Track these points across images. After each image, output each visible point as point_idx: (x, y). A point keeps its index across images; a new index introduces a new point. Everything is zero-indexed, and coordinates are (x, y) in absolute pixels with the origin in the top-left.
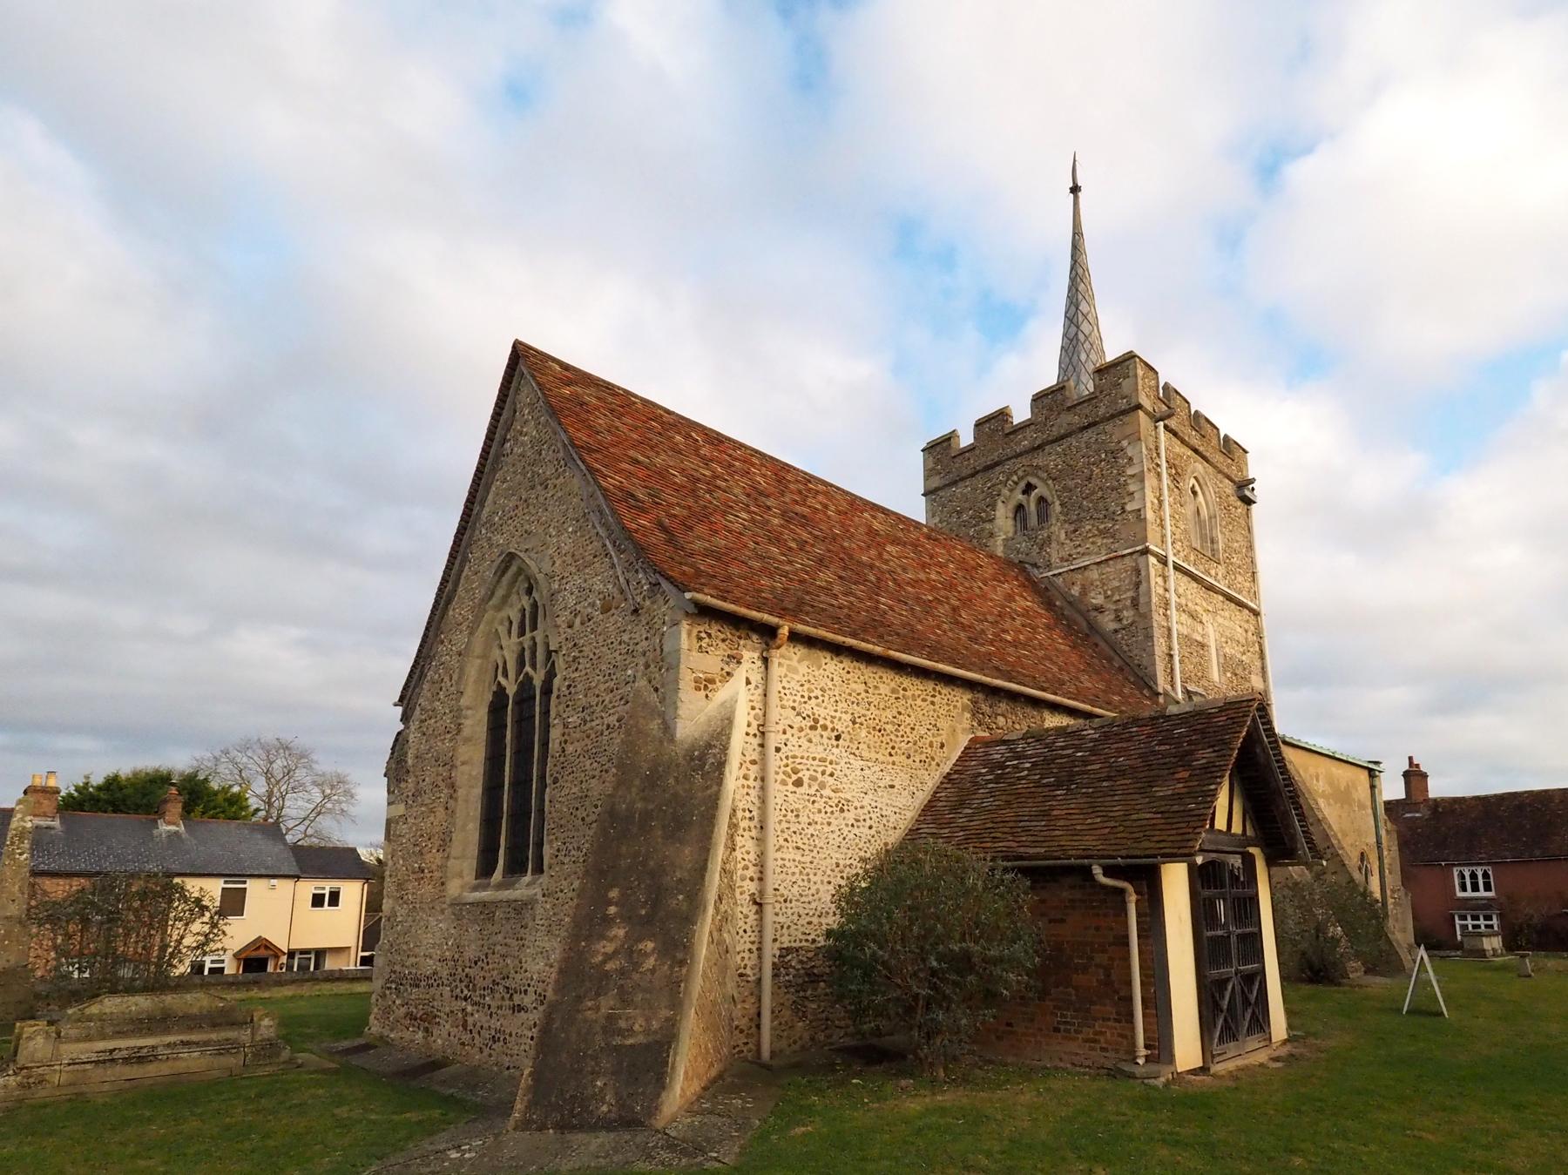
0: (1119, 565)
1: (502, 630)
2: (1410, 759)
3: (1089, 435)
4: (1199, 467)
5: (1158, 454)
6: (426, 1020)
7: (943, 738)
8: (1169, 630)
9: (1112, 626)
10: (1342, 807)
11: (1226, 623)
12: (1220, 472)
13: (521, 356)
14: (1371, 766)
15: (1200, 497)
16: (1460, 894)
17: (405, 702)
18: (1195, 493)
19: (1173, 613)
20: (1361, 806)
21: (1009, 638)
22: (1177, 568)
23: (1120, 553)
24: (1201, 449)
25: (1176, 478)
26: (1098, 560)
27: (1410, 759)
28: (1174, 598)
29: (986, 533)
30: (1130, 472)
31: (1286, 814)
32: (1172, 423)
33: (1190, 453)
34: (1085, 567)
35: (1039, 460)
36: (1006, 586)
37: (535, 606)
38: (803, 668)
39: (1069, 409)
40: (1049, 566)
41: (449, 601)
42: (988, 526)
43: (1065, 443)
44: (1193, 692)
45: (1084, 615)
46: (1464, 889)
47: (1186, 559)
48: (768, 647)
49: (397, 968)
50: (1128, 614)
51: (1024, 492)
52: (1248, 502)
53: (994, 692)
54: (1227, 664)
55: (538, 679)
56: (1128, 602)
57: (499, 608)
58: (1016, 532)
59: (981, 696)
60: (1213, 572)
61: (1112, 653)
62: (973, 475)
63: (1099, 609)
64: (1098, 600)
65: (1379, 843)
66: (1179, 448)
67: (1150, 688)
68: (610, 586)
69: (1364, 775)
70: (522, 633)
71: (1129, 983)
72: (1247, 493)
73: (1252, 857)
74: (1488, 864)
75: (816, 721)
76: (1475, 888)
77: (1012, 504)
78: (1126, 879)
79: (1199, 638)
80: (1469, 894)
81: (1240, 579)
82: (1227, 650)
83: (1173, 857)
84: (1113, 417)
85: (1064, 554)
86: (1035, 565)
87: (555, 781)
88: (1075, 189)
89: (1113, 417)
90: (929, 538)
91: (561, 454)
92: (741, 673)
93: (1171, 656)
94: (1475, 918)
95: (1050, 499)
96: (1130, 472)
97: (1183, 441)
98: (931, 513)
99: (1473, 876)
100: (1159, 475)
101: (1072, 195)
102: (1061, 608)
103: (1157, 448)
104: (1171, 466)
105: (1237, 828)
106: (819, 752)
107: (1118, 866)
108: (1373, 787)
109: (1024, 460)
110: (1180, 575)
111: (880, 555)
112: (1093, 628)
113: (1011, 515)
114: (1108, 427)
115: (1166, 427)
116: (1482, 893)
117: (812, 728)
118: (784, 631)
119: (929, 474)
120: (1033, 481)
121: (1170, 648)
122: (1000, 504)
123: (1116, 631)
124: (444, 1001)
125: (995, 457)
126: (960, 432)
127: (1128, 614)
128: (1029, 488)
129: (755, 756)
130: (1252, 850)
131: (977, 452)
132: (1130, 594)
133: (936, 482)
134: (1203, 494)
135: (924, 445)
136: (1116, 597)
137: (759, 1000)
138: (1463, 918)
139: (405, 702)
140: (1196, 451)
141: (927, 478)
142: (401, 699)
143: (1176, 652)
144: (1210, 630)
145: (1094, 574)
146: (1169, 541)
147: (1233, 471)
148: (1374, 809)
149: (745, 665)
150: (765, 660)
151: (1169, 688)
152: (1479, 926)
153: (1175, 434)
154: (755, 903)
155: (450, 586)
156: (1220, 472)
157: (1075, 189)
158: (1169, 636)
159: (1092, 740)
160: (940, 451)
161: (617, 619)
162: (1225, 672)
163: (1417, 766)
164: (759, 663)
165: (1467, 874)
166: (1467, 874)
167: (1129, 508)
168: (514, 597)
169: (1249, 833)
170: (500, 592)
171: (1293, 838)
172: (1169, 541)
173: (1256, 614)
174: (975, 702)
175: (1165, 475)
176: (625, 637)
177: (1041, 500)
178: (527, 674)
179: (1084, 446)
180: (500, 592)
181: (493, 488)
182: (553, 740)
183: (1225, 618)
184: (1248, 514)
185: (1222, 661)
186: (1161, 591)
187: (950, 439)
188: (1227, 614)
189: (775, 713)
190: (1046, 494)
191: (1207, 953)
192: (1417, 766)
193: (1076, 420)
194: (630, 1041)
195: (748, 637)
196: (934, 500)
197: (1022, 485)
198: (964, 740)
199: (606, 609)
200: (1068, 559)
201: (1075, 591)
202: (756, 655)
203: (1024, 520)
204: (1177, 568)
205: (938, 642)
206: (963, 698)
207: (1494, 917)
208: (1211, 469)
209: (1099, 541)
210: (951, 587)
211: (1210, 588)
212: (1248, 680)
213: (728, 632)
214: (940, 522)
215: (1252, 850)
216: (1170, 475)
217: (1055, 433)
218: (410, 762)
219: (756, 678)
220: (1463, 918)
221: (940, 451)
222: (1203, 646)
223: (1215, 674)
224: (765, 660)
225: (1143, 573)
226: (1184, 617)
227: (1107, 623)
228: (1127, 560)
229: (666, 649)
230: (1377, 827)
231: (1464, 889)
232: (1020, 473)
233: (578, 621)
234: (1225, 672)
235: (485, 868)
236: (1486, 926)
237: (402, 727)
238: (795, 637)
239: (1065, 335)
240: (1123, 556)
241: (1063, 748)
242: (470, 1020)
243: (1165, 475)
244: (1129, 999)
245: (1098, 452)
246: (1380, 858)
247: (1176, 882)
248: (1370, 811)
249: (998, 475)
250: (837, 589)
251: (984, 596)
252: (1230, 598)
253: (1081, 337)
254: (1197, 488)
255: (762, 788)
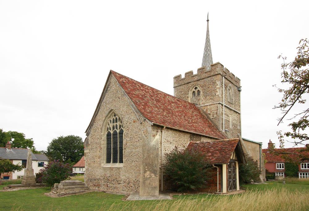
0: (214, 106)
1: (109, 122)
2: (270, 140)
3: (209, 79)
4: (230, 85)
5: (223, 83)
6: (99, 186)
7: (186, 142)
8: (223, 119)
9: (212, 117)
10: (253, 152)
11: (234, 116)
12: (235, 85)
13: (111, 73)
14: (260, 143)
15: (230, 91)
16: (277, 169)
17: (87, 132)
18: (229, 90)
19: (224, 115)
20: (257, 151)
21: (194, 121)
22: (225, 106)
23: (214, 103)
24: (231, 81)
25: (226, 88)
26: (210, 104)
27: (270, 140)
28: (224, 112)
29: (187, 97)
30: (217, 87)
31: (242, 157)
32: (226, 77)
33: (229, 82)
34: (207, 106)
35: (199, 83)
36: (192, 110)
37: (116, 118)
38: (166, 132)
39: (205, 73)
40: (200, 104)
41: (96, 115)
42: (187, 95)
43: (204, 80)
44: (227, 131)
45: (207, 115)
46: (278, 167)
47: (227, 104)
48: (162, 130)
49: (90, 178)
50: (215, 115)
51: (195, 89)
52: (240, 91)
53: (194, 134)
54: (233, 125)
55: (118, 131)
56: (215, 113)
57: (108, 118)
58: (193, 97)
59: (191, 135)
60: (232, 106)
61: (212, 123)
62: (184, 84)
63: (210, 114)
64: (209, 112)
65: (260, 159)
66: (227, 81)
67: (219, 130)
68: (135, 118)
69: (258, 146)
70: (113, 122)
71: (217, 181)
72: (240, 89)
73: (236, 163)
74: (283, 163)
75: (168, 141)
76: (280, 167)
77: (192, 91)
78: (218, 166)
79: (228, 120)
80: (279, 168)
81: (237, 107)
82: (233, 122)
83: (225, 163)
84: (214, 75)
85: (203, 102)
86: (197, 104)
87: (125, 149)
88: (208, 21)
89: (214, 75)
90: (178, 100)
91: (123, 93)
92: (158, 134)
93: (223, 124)
94: (280, 173)
95: (200, 91)
96: (217, 87)
97: (228, 80)
98: (175, 92)
99: (280, 165)
100: (223, 88)
101: (207, 22)
102: (202, 113)
103: (223, 82)
104: (225, 85)
105: (234, 159)
106: (168, 145)
107: (217, 164)
108: (260, 147)
109: (195, 83)
110: (225, 107)
111: (171, 106)
112: (208, 117)
113: (192, 93)
114: (213, 77)
115: (225, 77)
116: (282, 168)
117: (168, 142)
118: (165, 127)
119: (175, 83)
120: (197, 87)
121: (223, 122)
122: (190, 91)
123: (213, 119)
124: (102, 183)
125: (189, 81)
126: (182, 75)
127: (215, 115)
128: (196, 88)
129: (160, 147)
130: (236, 162)
131: (185, 79)
132: (215, 112)
133: (176, 85)
134: (231, 90)
135: (174, 77)
136: (213, 112)
137: (161, 183)
138: (277, 173)
139: (87, 132)
140: (230, 81)
141: (174, 84)
142: (86, 132)
143: (224, 123)
144: (230, 118)
145: (209, 107)
146: (224, 101)
147: (237, 85)
148: (260, 152)
149: (159, 132)
150: (162, 132)
151: (222, 130)
152: (278, 175)
153: (226, 79)
154: (160, 169)
155: (96, 112)
156: (235, 85)
157: (208, 21)
158: (223, 120)
159: (212, 144)
160: (177, 78)
161: (138, 124)
162: (233, 126)
163: (271, 142)
164: (161, 132)
165: (282, 165)
166: (282, 165)
167: (216, 94)
168: (112, 117)
169: (236, 159)
170: (109, 115)
171: (243, 160)
172: (224, 101)
173: (239, 114)
174: (190, 136)
175: (224, 87)
176: (139, 127)
177: (198, 91)
178: (115, 130)
179: (208, 81)
180: (109, 115)
181: (106, 96)
182: (124, 142)
183: (233, 115)
184: (239, 94)
185: (232, 124)
186: (222, 111)
187: (179, 76)
188: (234, 114)
189: (163, 140)
190: (200, 90)
191: (229, 178)
192: (271, 142)
193: (207, 75)
194: (153, 186)
195: (159, 128)
196: (176, 89)
197: (195, 87)
198: (189, 143)
199: (134, 122)
200: (204, 103)
201: (205, 110)
202: (160, 131)
203: (195, 94)
204: (225, 106)
205: (184, 124)
206: (189, 135)
207: (284, 173)
208: (233, 85)
209: (210, 101)
210: (183, 111)
211: (231, 110)
212: (237, 127)
213: (157, 128)
214: (177, 93)
215: (236, 162)
216: (225, 87)
217: (202, 77)
218: (89, 143)
219: (160, 134)
220: (277, 173)
221: (177, 78)
222: (229, 121)
223: (231, 127)
224: (162, 132)
225: (218, 108)
226: (226, 116)
227: (211, 117)
228: (215, 105)
229: (148, 130)
230: (260, 156)
231: (278, 167)
232: (194, 85)
233: (128, 123)
234: (233, 126)
235: (108, 161)
236: (279, 175)
237: (86, 137)
238: (167, 128)
239: (204, 54)
240: (215, 104)
241: (207, 145)
242: (109, 185)
243: (224, 87)
244: (217, 183)
245: (211, 82)
246: (260, 161)
247: (225, 167)
248: (259, 152)
249: (190, 85)
250: (167, 115)
251: (188, 113)
252: (234, 111)
253: (207, 54)
254: (230, 89)
255: (161, 151)
